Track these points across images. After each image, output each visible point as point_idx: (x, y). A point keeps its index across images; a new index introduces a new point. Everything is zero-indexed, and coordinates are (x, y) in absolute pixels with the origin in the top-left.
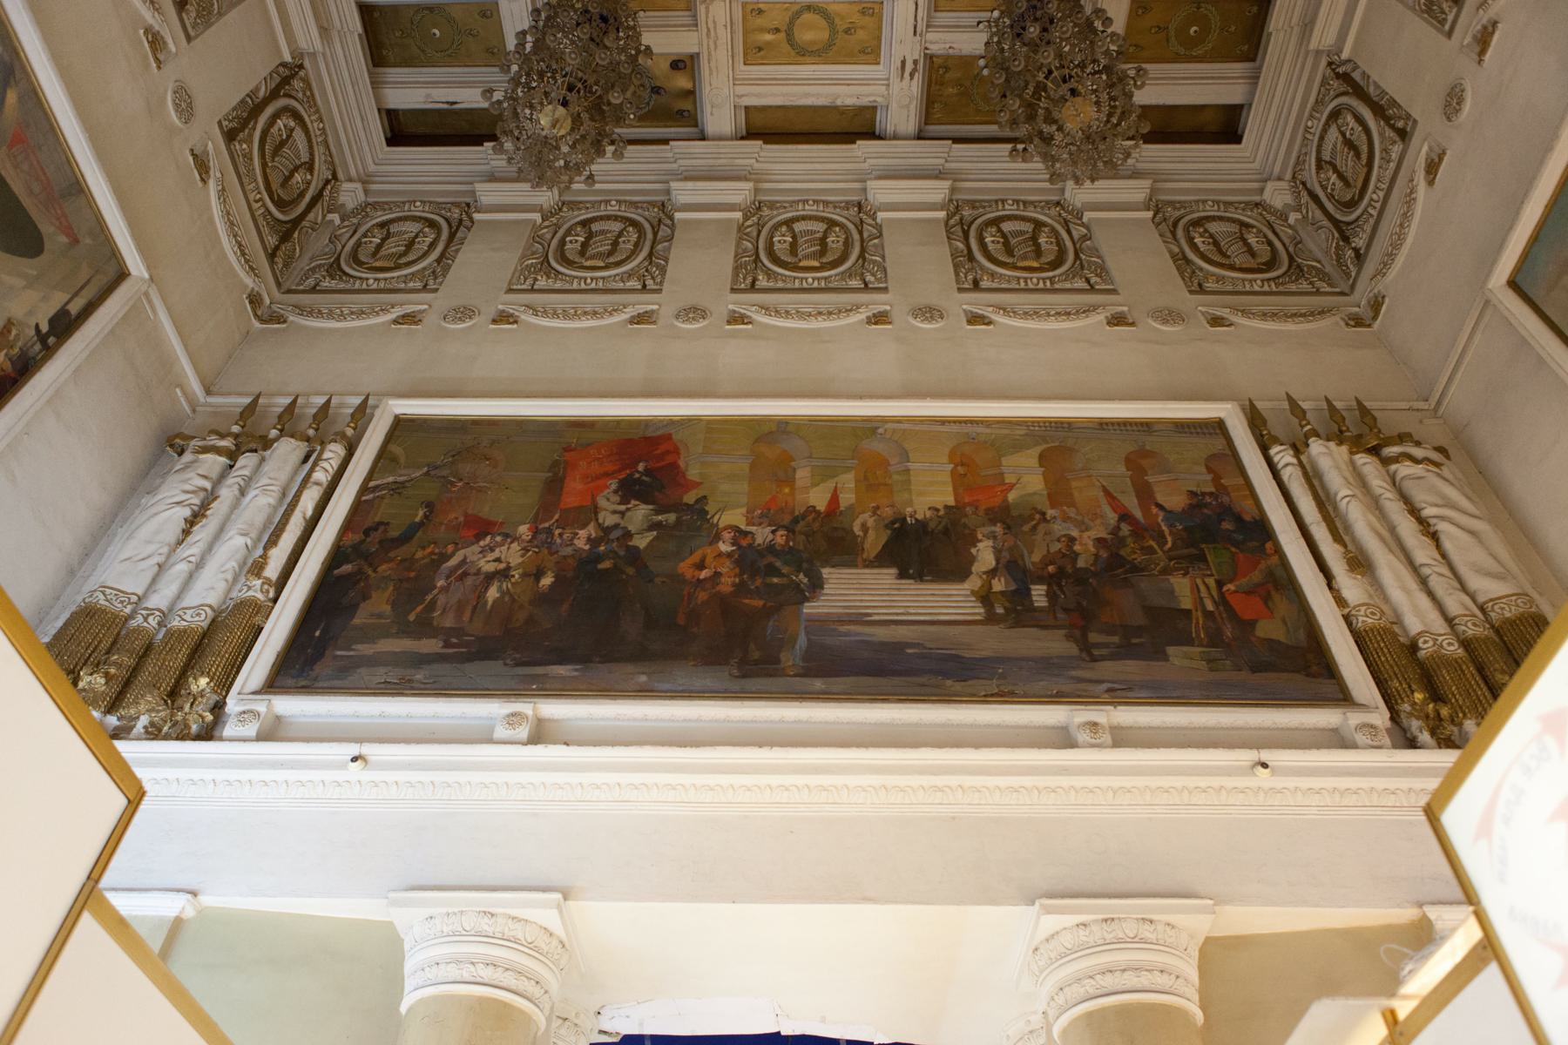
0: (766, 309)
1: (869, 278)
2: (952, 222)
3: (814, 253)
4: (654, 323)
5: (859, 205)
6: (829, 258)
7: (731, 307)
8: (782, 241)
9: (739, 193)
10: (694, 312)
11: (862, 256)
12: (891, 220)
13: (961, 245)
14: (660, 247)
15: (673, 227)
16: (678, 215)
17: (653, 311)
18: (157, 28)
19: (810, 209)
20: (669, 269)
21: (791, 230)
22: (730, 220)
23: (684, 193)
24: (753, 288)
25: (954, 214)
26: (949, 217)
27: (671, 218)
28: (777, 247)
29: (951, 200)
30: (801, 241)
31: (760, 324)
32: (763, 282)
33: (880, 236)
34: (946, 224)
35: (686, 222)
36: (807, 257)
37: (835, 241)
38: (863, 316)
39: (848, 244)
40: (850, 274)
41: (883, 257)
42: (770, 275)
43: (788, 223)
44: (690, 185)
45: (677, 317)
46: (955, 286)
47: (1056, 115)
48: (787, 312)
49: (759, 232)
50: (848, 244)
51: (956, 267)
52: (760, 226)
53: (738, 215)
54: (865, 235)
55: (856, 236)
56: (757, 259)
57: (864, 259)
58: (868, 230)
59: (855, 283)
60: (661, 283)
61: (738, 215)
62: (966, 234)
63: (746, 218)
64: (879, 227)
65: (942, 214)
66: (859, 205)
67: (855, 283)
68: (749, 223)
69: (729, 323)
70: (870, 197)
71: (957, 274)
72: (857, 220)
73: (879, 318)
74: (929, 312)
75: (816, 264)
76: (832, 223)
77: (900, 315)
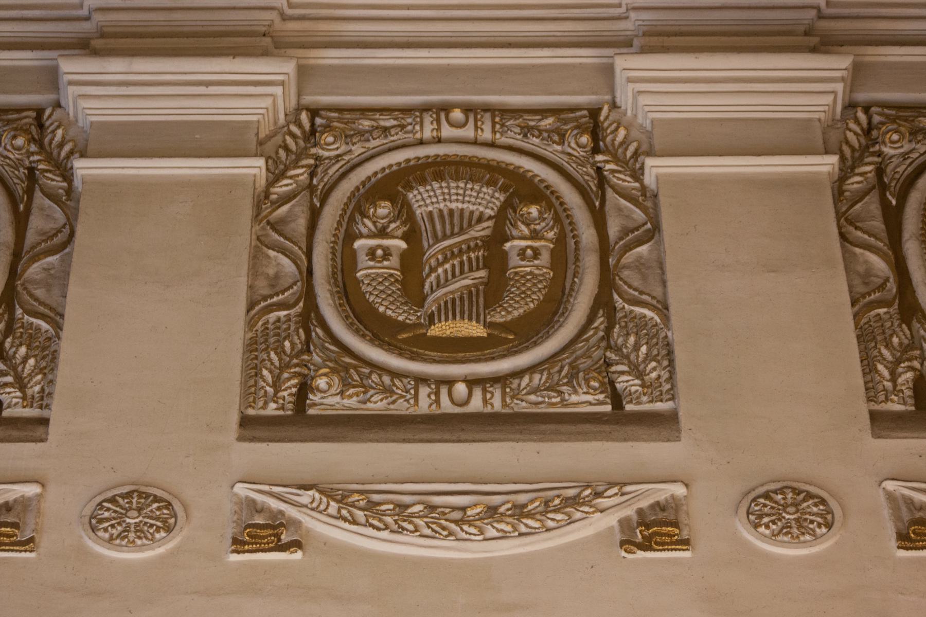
0: (340, 497)
1: (626, 382)
2: (855, 183)
3: (470, 293)
4: (28, 544)
5: (593, 123)
6: (513, 309)
7: (242, 490)
8: (378, 254)
9: (255, 91)
10: (136, 509)
11: (603, 302)
12: (681, 183)
13: (879, 264)
14: (34, 270)
15: (68, 201)
16: (83, 168)
17: (24, 503)
18: (630, 512)
19: (455, 138)
20: (67, 349)
21: (404, 212)
22: (229, 184)
23: (98, 92)
24: (300, 422)
25: (858, 161)
26: (846, 171)
27: (67, 175)
28: (365, 269)
29: (851, 106)
30: (433, 251)
31: (328, 546)
32: (328, 397)
33: (654, 232)
34: (838, 193)
35: (113, 189)
36: (451, 309)
37: (527, 250)
38: (611, 520)
39: (563, 257)
40: (564, 368)
41: (663, 308)
42: (349, 368)
43: (392, 187)
44: (116, 67)
45: (94, 524)
46: (863, 409)
47: (879, 281)
48: (371, 506)
49: (314, 215)
50: (563, 257)
51: (865, 337)
52: (317, 197)
53: (254, 168)
54: (613, 230)
55: (588, 235)
56: (311, 315)
57: (611, 311)
58: (622, 213)
59: (586, 399)
60: (45, 397)
61: (254, 168)
62: (893, 219)
63: (275, 177)
64: (647, 199)
65: (827, 164)
66: (593, 123)
67: (586, 399)
68: (284, 187)
69: (238, 545)
70: (625, 95)
71: (868, 367)
72: (586, 174)
73: (656, 529)
74: (790, 506)
75: (476, 330)
76: (521, 189)
77: (716, 520)
